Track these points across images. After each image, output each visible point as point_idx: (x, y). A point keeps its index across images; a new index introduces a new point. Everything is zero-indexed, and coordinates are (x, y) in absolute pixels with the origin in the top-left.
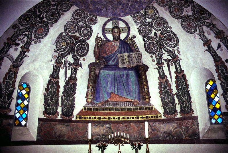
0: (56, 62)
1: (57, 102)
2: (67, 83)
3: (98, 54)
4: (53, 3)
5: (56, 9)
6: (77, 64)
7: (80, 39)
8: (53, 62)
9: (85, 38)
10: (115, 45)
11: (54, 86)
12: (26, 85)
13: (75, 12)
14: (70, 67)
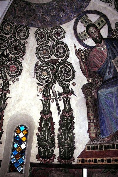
0: (44, 96)
1: (53, 142)
2: (62, 117)
3: (87, 71)
4: (8, 36)
5: (16, 41)
6: (68, 91)
7: (59, 61)
8: (41, 97)
9: (64, 57)
10: (101, 49)
11: (47, 124)
12: (24, 127)
13: (36, 34)
14: (60, 98)
